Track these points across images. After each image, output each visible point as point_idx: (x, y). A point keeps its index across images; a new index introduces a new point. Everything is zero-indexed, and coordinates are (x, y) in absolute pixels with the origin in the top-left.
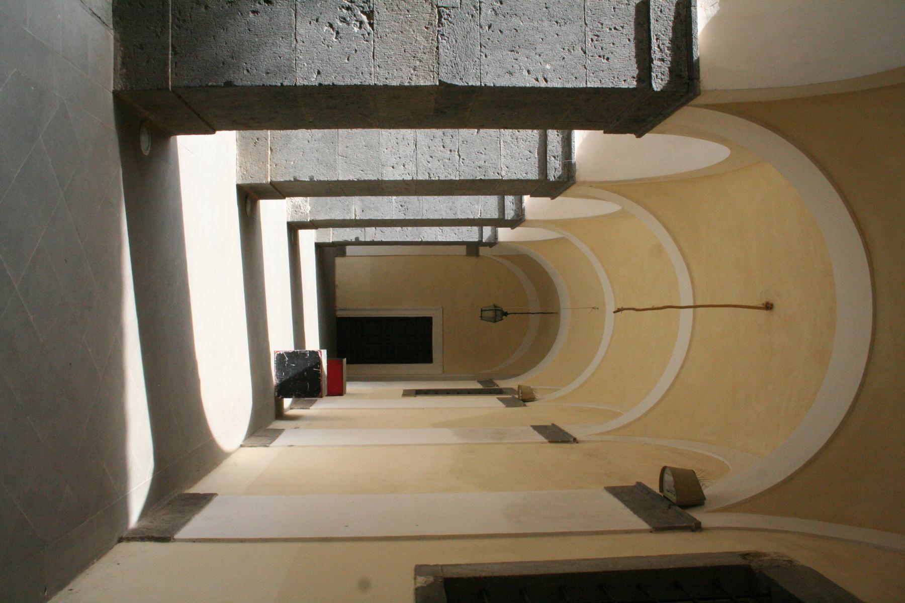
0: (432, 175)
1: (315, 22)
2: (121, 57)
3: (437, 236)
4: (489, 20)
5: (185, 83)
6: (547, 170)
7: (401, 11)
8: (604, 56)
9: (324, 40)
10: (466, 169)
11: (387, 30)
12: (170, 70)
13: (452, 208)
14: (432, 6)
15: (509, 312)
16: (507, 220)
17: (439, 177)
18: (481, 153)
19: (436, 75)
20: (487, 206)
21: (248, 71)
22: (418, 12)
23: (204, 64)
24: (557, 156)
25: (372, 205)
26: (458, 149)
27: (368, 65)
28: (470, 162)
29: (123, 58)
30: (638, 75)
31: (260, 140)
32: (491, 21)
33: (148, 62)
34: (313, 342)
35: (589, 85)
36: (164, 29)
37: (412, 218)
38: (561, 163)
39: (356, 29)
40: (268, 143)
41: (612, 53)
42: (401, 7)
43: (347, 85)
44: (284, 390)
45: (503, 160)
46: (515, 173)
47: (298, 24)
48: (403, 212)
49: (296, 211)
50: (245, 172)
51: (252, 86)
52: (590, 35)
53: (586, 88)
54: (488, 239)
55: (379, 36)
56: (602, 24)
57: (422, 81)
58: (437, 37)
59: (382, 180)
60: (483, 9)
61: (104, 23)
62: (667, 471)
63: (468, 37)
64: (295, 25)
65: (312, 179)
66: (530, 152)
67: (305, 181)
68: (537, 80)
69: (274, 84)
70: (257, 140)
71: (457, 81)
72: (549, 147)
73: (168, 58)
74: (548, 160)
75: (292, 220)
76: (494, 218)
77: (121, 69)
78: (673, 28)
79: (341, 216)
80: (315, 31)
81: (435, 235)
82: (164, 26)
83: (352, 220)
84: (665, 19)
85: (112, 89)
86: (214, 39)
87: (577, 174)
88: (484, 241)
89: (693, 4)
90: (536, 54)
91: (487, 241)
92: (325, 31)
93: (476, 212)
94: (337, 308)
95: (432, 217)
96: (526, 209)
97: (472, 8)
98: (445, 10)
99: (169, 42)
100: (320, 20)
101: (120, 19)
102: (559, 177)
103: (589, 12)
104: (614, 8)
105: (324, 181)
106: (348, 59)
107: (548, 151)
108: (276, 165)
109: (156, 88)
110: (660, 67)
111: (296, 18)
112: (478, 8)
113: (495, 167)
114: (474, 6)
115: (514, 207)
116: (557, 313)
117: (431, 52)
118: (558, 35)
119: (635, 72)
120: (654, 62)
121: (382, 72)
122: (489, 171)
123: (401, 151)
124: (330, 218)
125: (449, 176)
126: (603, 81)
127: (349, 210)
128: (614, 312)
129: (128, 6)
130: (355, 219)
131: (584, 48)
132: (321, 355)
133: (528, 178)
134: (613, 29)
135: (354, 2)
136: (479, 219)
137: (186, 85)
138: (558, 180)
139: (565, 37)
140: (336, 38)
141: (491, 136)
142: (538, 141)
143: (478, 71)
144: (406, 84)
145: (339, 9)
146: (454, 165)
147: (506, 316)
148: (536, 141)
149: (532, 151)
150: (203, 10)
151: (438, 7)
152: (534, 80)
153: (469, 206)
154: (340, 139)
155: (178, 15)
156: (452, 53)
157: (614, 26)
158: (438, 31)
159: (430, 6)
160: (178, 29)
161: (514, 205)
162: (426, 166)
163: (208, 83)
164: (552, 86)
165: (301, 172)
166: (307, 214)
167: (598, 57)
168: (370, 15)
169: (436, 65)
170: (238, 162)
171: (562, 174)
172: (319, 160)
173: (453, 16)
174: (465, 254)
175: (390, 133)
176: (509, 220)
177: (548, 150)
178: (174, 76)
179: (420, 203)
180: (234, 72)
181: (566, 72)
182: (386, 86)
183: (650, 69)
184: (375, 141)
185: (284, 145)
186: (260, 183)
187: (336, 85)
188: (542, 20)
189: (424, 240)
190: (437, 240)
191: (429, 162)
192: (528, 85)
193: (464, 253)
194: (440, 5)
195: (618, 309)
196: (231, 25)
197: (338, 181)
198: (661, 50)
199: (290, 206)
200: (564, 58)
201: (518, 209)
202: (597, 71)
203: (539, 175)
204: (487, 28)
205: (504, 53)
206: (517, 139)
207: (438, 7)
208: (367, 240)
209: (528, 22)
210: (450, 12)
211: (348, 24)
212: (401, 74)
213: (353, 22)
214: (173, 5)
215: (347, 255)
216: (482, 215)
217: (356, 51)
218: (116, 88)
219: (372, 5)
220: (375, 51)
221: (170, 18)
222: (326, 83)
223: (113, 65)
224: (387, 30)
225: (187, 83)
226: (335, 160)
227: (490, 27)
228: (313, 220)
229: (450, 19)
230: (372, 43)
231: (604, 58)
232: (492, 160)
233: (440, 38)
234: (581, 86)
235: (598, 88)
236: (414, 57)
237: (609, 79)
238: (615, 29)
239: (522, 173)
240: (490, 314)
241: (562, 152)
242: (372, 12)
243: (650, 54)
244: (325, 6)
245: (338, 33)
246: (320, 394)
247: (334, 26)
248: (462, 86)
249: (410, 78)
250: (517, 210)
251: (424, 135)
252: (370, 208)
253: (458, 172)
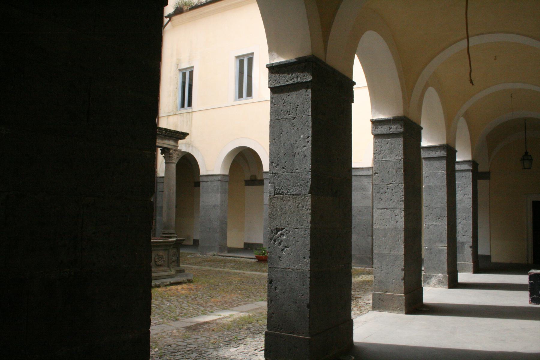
0: (401, 200)
1: (281, 258)
3: (469, 198)
6: (397, 133)
9: (289, 254)
11: (285, 221)
12: (301, 336)
14: (274, 198)
15: (525, 151)
17: (402, 196)
19: (306, 196)
21: (302, 295)
22: (277, 205)
24: (390, 127)
25: (439, 237)
27: (301, 231)
30: (305, 89)
31: (380, 298)
32: (281, 167)
34: (524, 279)
35: (310, 114)
38: (393, 125)
39: (284, 237)
40: (383, 294)
41: (295, 104)
42: (275, 214)
43: (310, 243)
45: (392, 159)
46: (400, 151)
47: (281, 267)
48: (443, 218)
50: (399, 309)
52: (287, 116)
55: (288, 225)
56: (282, 110)
57: (309, 203)
58: (289, 195)
60: (276, 171)
63: (288, 179)
64: (282, 268)
65: (403, 270)
66: (388, 143)
67: (404, 274)
68: (308, 142)
70: (381, 300)
71: (309, 184)
72: (385, 132)
73: (295, 336)
74: (392, 133)
75: (447, 285)
79: (445, 255)
80: (285, 258)
81: (468, 199)
84: (279, 78)
86: (287, 311)
87: (400, 115)
88: (471, 169)
89: (272, 65)
90: (296, 143)
91: (472, 166)
92: (285, 254)
93: (442, 173)
95: (446, 200)
97: (275, 177)
98: (276, 191)
99: (288, 335)
100: (280, 256)
102: (401, 125)
103: (276, 117)
104: (275, 105)
105: (404, 263)
106: (298, 242)
107: (387, 133)
108: (395, 290)
110: (301, 78)
111: (278, 268)
112: (275, 174)
113: (396, 163)
117: (295, 198)
118: (287, 133)
119: (304, 90)
120: (298, 81)
121: (304, 224)
123: (388, 217)
124: (446, 262)
125: (402, 190)
126: (308, 107)
127: (441, 250)
130: (447, 247)
131: (293, 118)
133: (402, 144)
134: (284, 104)
135: (272, 238)
136: (446, 172)
138: (403, 126)
140: (288, 248)
142: (382, 139)
143: (304, 173)
144: (310, 211)
145: (275, 246)
146: (396, 187)
148: (382, 140)
149: (387, 142)
150: (274, 315)
151: (274, 195)
152: (308, 143)
154: (381, 252)
156: (296, 187)
157: (282, 104)
158: (285, 195)
159: (274, 199)
160: (282, 329)
161: (438, 151)
162: (396, 203)
164: (311, 134)
166: (444, 276)
168: (278, 230)
169: (301, 196)
171: (400, 124)
173: (279, 187)
175: (378, 223)
177: (386, 133)
178: (304, 335)
179: (437, 208)
180: (303, 303)
181: (304, 127)
182: (311, 223)
187: (310, 249)
188: (281, 141)
190: (471, 198)
191: (394, 201)
192: (311, 146)
194: (273, 194)
195: (470, 83)
196: (281, 302)
197: (405, 254)
198: (293, 78)
199: (438, 286)
200: (298, 128)
201: (440, 148)
202: (304, 111)
203: (400, 137)
204: (284, 169)
205: (296, 160)
206: (381, 151)
207: (274, 195)
208: (472, 241)
209: (281, 148)
211: (282, 241)
212: (305, 214)
213: (281, 238)
215: (488, 254)
216: (444, 170)
219: (273, 229)
220: (295, 228)
221: (277, 332)
222: (309, 254)
224: (285, 221)
226: (393, 255)
227: (284, 168)
229: (280, 189)
230: (291, 229)
232: (392, 165)
233: (289, 193)
234: (311, 118)
236: (297, 207)
238: (284, 103)
241: (387, 125)
242: (276, 228)
243: (295, 84)
244: (273, 253)
245: (286, 247)
247: (283, 249)
248: (311, 182)
249: (308, 209)
250: (441, 149)
251: (379, 204)
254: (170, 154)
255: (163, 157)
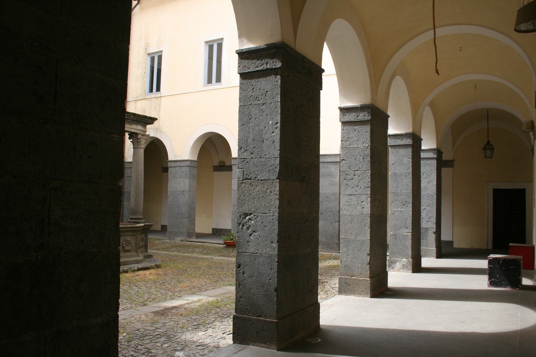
0: (368, 186)
2: (262, 344)
4: (249, 154)
5: (275, 312)
7: (244, 199)
8: (266, 94)
9: (257, 239)
10: (365, 166)
13: (405, 175)
14: (242, 183)
15: (487, 141)
16: (412, 143)
17: (369, 182)
18: (356, 158)
20: (404, 155)
21: (270, 279)
23: (267, 301)
24: (357, 115)
25: (404, 223)
26: (353, 171)
28: (361, 164)
29: (262, 343)
33: (264, 331)
34: (483, 264)
35: (279, 100)
36: (250, 320)
37: (411, 199)
39: (253, 222)
41: (264, 90)
42: (243, 199)
43: (278, 228)
44: (516, 283)
45: (359, 146)
47: (249, 251)
49: (406, 267)
51: (278, 278)
52: (256, 102)
53: (281, 102)
54: (435, 155)
56: (251, 96)
58: (257, 180)
59: (370, 214)
60: (244, 157)
61: (243, 349)
62: (518, 28)
63: (256, 164)
66: (355, 131)
68: (277, 128)
69: (277, 266)
71: (277, 170)
72: (352, 120)
73: (263, 320)
76: (411, 151)
77: (267, 345)
78: (252, 60)
80: (253, 243)
82: (249, 320)
83: (412, 234)
85: (276, 351)
86: (255, 295)
87: (367, 103)
89: (241, 51)
91: (436, 155)
94: (486, 248)
95: (411, 187)
96: (406, 132)
98: (244, 176)
100: (248, 241)
101: (245, 341)
102: (369, 113)
104: (244, 91)
106: (266, 227)
107: (355, 120)
109: (276, 328)
110: (270, 64)
114: (243, 162)
115: (405, 139)
116: (488, 110)
118: (256, 119)
119: (273, 76)
120: (268, 67)
122: (366, 153)
123: (355, 203)
128: (439, 75)
129: (239, 336)
130: (412, 232)
132: (491, 257)
133: (369, 131)
137: (276, 312)
138: (370, 114)
139: (257, 114)
140: (256, 233)
141: (347, 153)
142: (349, 126)
143: (272, 159)
144: (278, 197)
147: (490, 142)
150: (242, 299)
151: (243, 180)
153: (405, 166)
155: (244, 312)
156: (264, 173)
157: (252, 90)
158: (254, 180)
163: (275, 301)
165: (365, 260)
166: (408, 261)
167: (266, 97)
168: (246, 215)
169: (270, 181)
170: (358, 296)
172: (359, 250)
173: (247, 172)
174: (452, 168)
176: (413, 141)
178: (271, 318)
180: (271, 286)
182: (279, 208)
183: (272, 69)
184: (349, 218)
185: (349, 269)
186: (370, 284)
187: (278, 233)
188: (249, 127)
189: (436, 193)
191: (361, 188)
193: (451, 169)
195: (436, 72)
196: (249, 286)
198: (262, 65)
199: (402, 270)
200: (267, 114)
203: (368, 125)
204: (253, 155)
207: (243, 180)
208: (435, 227)
209: (250, 134)
210: (245, 174)
211: (250, 226)
212: (273, 199)
214: (239, 314)
215: (452, 240)
217: (262, 223)
218: (275, 349)
219: (242, 214)
220: (263, 212)
221: (245, 316)
222: (277, 239)
223: (265, 349)
225: (275, 312)
226: (359, 241)
227: (252, 154)
228: (412, 258)
229: (248, 174)
231: (267, 94)
234: (280, 104)
235: (281, 96)
236: (266, 192)
237: (276, 90)
238: (253, 89)
239: (367, 135)
240: (488, 152)
241: (355, 112)
242: (245, 213)
243: (264, 70)
244: (241, 237)
245: (254, 232)
246: (518, 260)
247: (251, 233)
251: (346, 190)
252: (405, 223)
253: (366, 171)
254: (138, 139)
255: (131, 142)
